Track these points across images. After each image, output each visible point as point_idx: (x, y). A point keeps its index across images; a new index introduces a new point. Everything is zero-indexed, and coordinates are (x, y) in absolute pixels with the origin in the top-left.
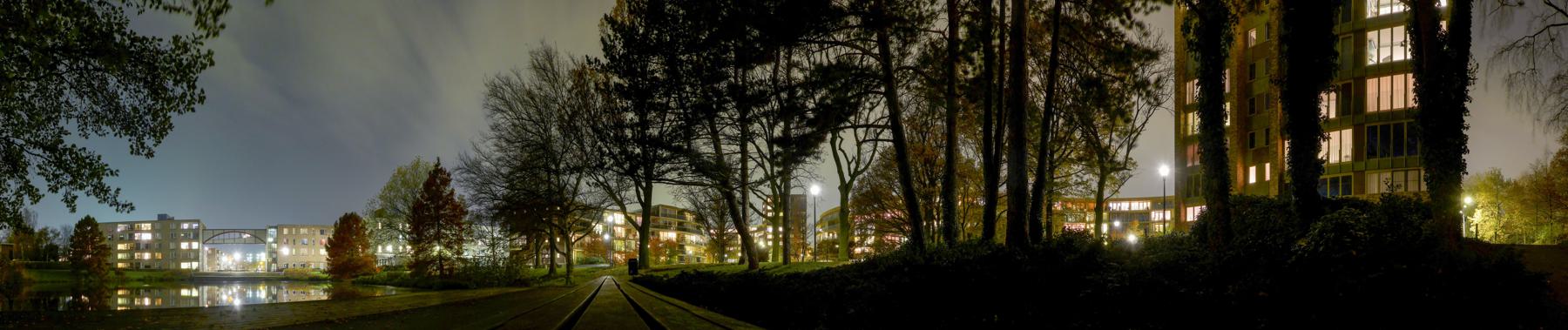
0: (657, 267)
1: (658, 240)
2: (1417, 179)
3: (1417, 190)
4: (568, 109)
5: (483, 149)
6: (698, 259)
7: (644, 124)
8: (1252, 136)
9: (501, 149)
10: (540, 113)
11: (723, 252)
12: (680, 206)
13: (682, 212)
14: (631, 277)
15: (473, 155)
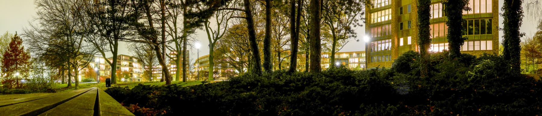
0: (120, 83)
5: (34, 25)
7: (114, 11)
8: (402, 24)
9: (43, 25)
10: (62, 7)
12: (131, 55)
14: (106, 88)
15: (30, 28)
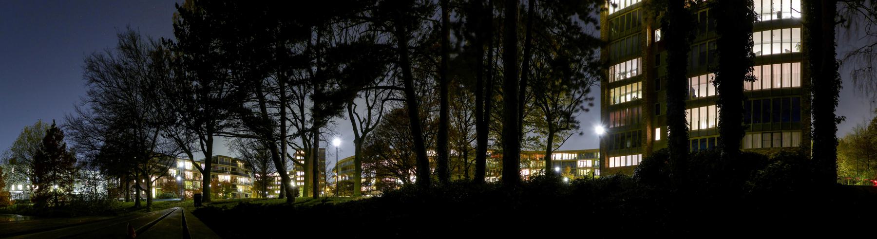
1: (217, 181)
2: (780, 138)
3: (780, 146)
4: (149, 81)
6: (247, 195)
7: (207, 89)
8: (658, 106)
9: (97, 110)
10: (126, 83)
11: (266, 190)
12: (233, 156)
13: (234, 161)
15: (76, 116)
